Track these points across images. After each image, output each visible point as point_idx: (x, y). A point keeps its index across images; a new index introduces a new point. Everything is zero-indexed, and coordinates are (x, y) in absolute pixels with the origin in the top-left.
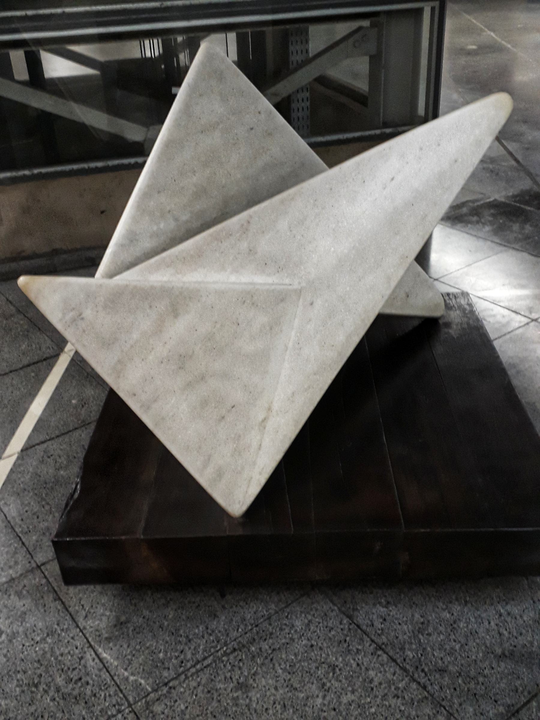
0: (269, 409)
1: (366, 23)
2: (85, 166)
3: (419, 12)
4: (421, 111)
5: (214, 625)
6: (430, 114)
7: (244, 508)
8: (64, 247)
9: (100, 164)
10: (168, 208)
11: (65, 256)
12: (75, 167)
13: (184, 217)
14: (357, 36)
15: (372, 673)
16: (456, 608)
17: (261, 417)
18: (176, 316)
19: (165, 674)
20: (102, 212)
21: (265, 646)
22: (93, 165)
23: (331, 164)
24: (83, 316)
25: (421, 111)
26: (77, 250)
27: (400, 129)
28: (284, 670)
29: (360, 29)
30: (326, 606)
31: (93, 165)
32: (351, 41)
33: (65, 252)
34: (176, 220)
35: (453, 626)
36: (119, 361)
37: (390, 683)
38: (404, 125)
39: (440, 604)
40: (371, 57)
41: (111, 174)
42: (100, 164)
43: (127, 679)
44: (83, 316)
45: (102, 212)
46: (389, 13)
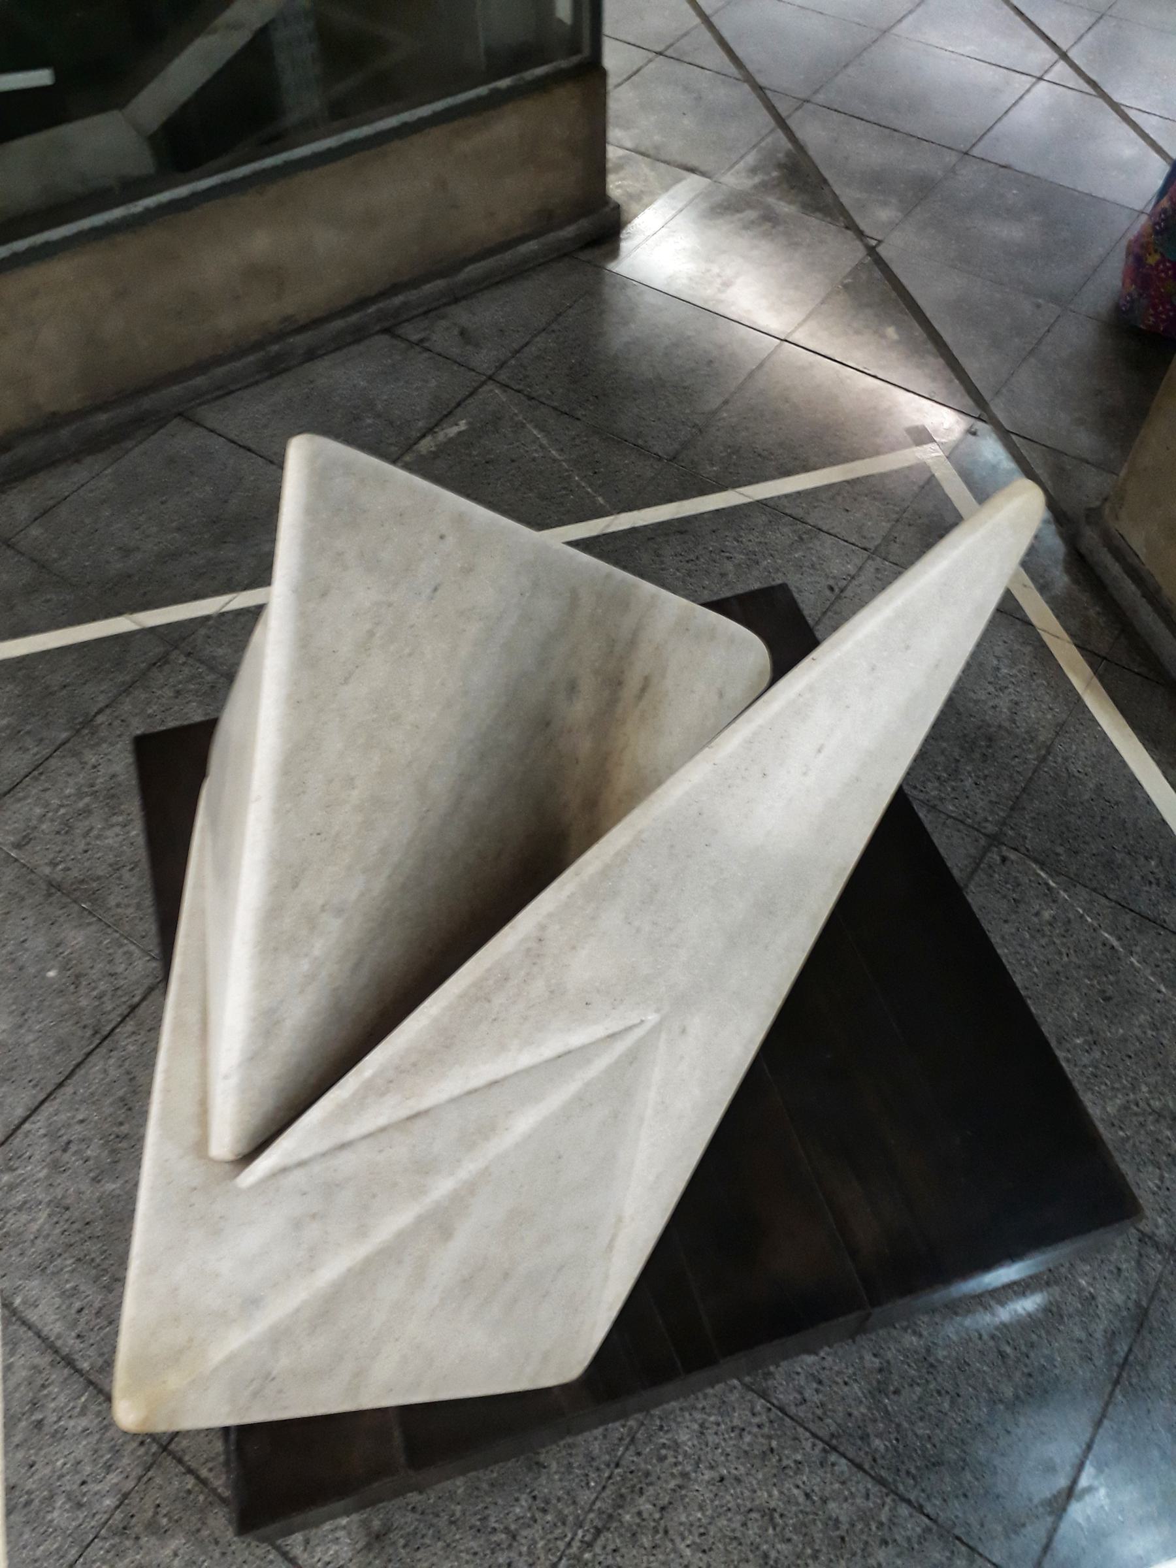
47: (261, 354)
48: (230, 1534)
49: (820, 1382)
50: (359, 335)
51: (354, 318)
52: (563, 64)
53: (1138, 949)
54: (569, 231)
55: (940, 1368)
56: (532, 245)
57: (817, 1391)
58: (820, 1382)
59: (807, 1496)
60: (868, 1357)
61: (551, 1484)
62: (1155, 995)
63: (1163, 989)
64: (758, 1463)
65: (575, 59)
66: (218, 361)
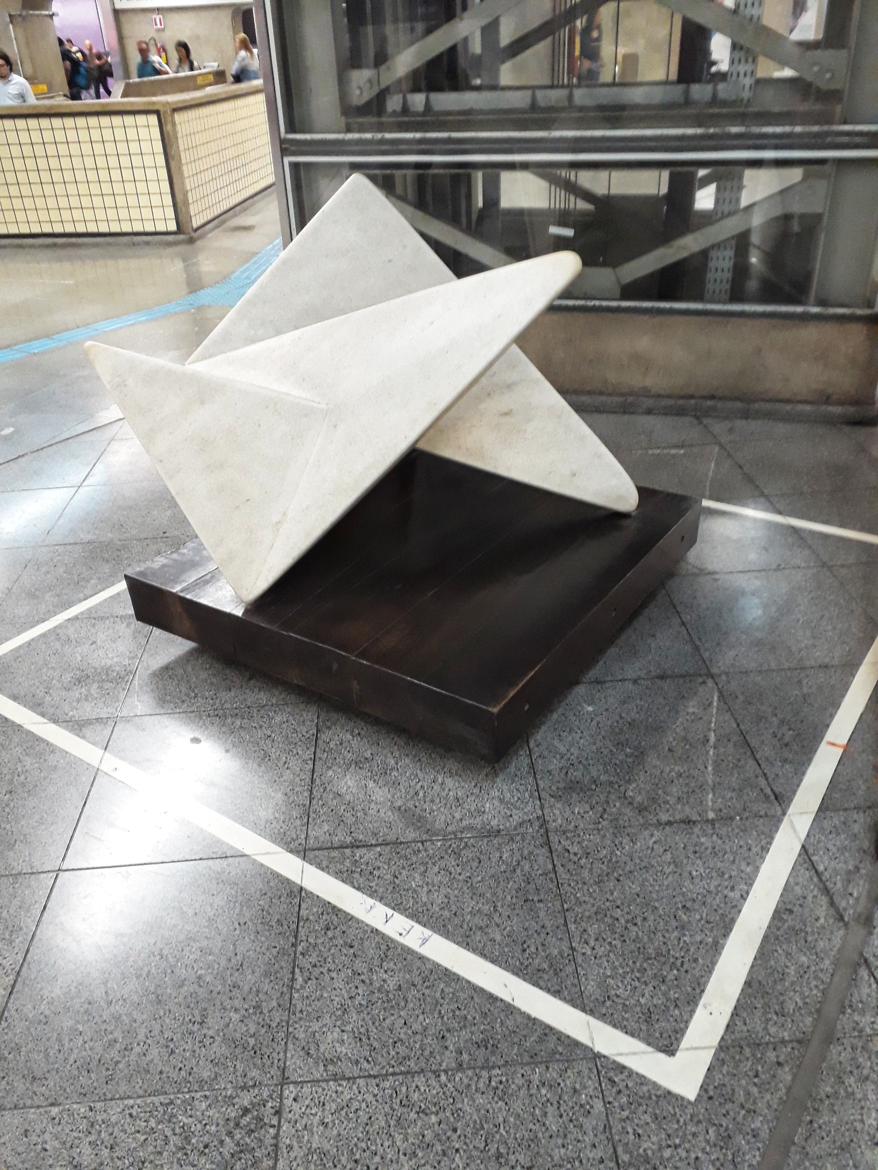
0: (285, 514)
47: (621, 399)
48: (150, 672)
49: (341, 744)
50: (681, 412)
51: (681, 402)
52: (859, 312)
53: (722, 750)
54: (838, 410)
55: (387, 776)
56: (808, 408)
57: (336, 745)
58: (341, 744)
59: (285, 763)
60: (369, 752)
61: (225, 695)
62: (702, 768)
63: (710, 768)
64: (286, 742)
65: (867, 312)
66: (601, 393)
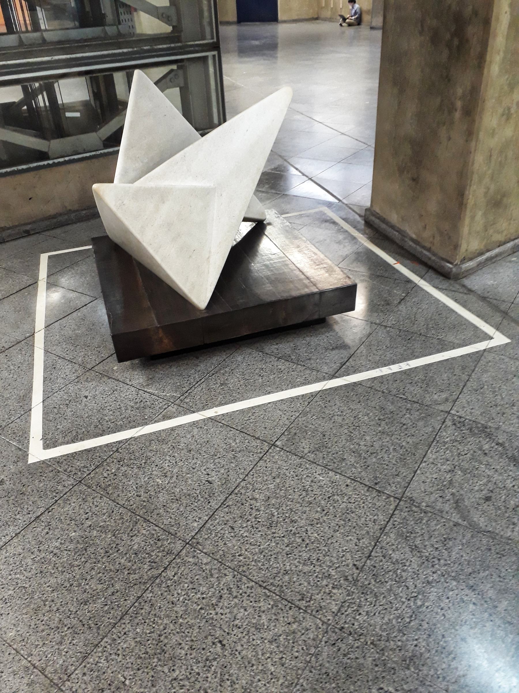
0: (210, 252)
1: (174, 67)
2: (15, 168)
3: (205, 58)
4: (216, 121)
5: (199, 368)
6: (222, 120)
7: (206, 304)
8: (8, 226)
9: (24, 167)
10: (137, 156)
11: (9, 231)
12: (8, 170)
13: (146, 161)
14: (171, 75)
15: (280, 367)
16: (308, 339)
17: (207, 256)
18: (164, 203)
19: (184, 389)
20: (30, 199)
21: (227, 369)
22: (20, 168)
23: (202, 135)
24: (124, 203)
25: (216, 121)
26: (16, 226)
27: (206, 131)
28: (240, 375)
29: (172, 71)
30: (250, 351)
31: (20, 168)
32: (168, 79)
33: (9, 229)
34: (142, 162)
35: (309, 344)
36: (142, 227)
37: (289, 368)
38: (209, 129)
39: (301, 339)
40: (181, 89)
41: (32, 173)
42: (24, 167)
43: (166, 395)
44: (124, 203)
45: (30, 199)
46: (189, 59)
